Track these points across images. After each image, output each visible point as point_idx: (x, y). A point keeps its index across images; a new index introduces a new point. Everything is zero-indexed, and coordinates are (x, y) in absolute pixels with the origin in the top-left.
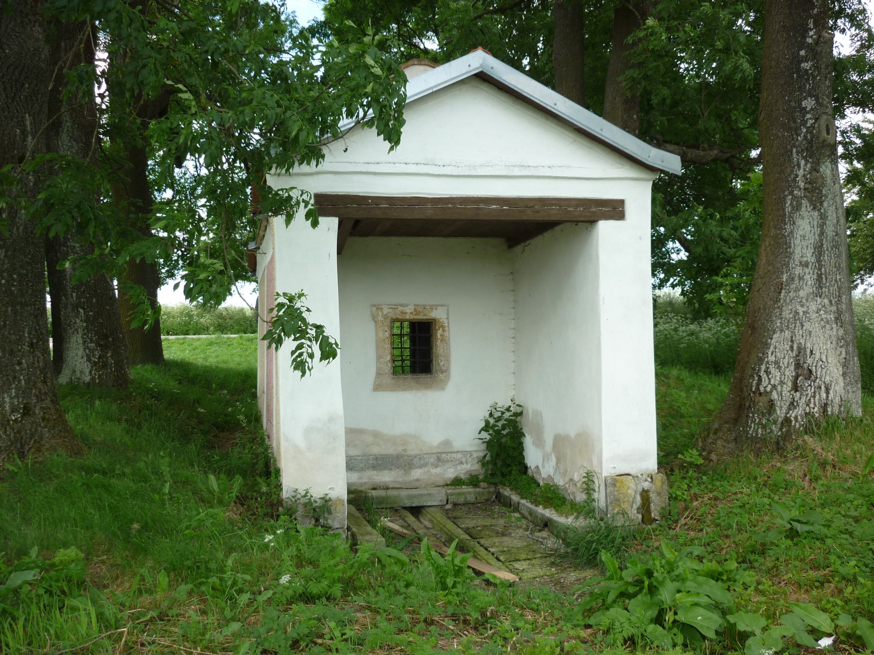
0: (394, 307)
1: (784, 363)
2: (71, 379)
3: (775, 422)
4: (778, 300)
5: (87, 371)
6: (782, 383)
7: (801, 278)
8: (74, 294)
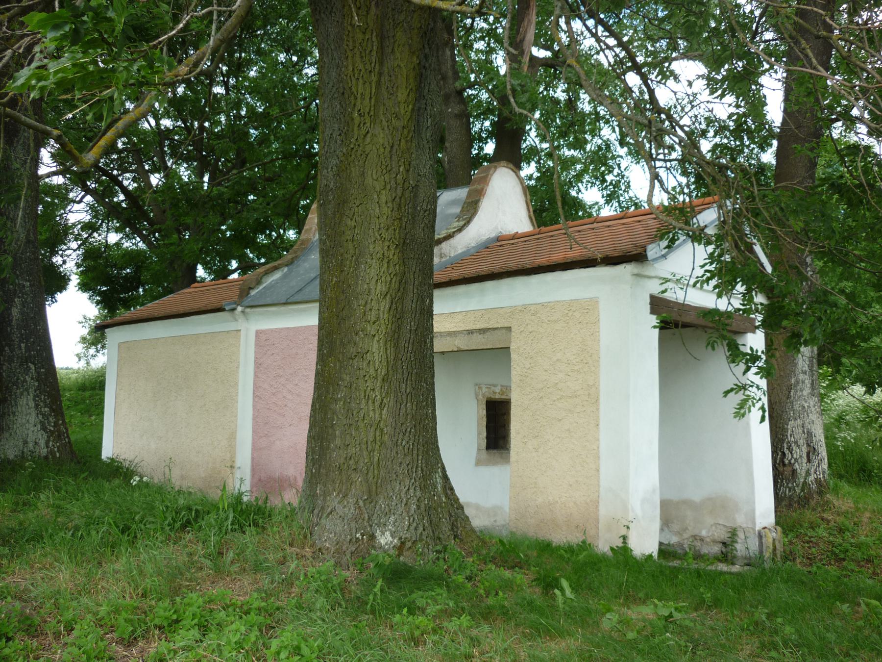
0: (489, 386)
1: (801, 442)
2: (23, 452)
3: (798, 486)
4: (789, 397)
5: (42, 443)
6: (801, 456)
7: (803, 382)
8: (23, 345)
